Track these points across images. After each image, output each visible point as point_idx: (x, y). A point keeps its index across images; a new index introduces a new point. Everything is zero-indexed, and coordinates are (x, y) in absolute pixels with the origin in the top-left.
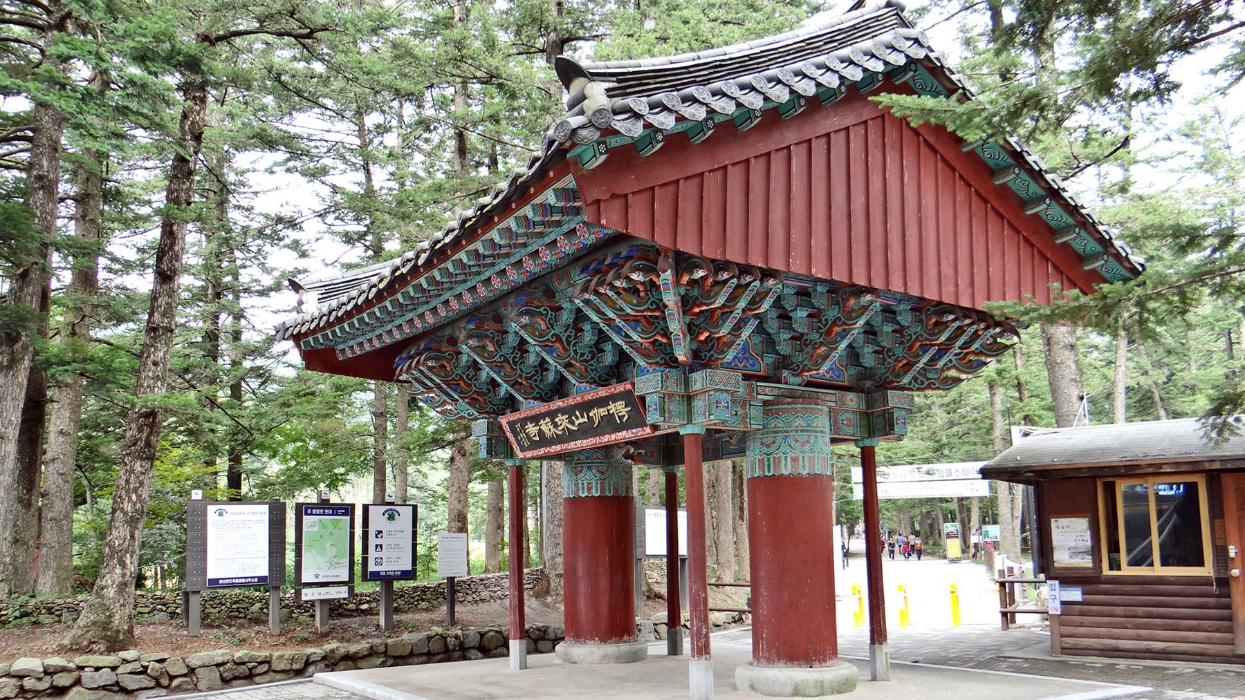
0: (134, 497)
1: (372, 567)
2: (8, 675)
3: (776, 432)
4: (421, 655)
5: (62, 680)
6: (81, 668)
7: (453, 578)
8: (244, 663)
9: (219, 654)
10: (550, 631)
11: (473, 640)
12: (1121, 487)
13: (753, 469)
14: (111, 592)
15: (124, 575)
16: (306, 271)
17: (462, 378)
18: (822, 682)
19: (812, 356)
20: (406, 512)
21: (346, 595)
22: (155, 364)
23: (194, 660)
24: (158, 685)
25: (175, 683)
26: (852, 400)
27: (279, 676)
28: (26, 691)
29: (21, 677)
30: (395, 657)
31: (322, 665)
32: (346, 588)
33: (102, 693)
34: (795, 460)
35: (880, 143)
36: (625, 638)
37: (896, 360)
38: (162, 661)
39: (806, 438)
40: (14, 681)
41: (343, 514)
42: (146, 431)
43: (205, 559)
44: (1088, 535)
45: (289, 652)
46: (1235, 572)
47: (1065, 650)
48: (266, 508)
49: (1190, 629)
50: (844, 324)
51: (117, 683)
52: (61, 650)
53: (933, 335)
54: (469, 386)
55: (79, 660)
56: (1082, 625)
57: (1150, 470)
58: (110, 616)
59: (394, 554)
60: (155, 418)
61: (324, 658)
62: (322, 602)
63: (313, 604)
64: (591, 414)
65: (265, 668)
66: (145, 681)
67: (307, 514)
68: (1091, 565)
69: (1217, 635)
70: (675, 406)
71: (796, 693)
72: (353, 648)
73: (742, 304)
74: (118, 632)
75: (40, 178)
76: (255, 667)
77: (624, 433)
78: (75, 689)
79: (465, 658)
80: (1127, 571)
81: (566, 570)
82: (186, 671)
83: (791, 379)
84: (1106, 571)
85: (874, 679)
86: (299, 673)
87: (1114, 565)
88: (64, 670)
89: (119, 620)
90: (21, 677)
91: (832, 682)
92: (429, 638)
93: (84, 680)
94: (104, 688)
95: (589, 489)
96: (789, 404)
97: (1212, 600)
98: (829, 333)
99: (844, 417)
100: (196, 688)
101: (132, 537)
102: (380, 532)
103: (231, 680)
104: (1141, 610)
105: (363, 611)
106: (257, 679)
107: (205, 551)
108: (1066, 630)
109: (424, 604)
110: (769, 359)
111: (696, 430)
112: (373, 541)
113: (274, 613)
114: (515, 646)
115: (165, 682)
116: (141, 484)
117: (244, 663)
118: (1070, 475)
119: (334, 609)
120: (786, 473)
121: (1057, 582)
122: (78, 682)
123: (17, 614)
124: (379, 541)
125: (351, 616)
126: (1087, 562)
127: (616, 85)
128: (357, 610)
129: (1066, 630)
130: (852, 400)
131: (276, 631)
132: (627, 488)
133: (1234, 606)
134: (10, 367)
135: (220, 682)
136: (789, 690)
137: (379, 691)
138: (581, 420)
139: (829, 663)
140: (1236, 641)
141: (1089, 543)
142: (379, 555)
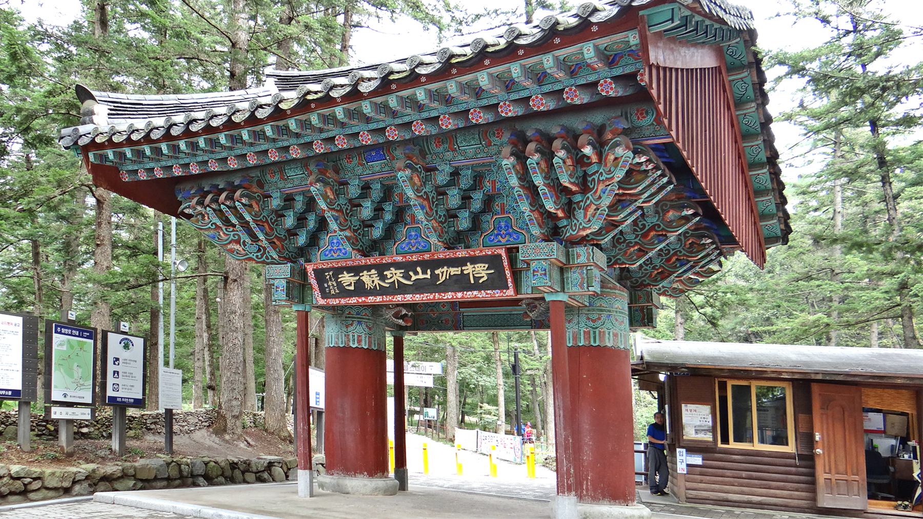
1: (110, 393)
3: (602, 310)
4: (163, 479)
7: (171, 410)
8: (19, 479)
10: (253, 464)
11: (200, 470)
12: (730, 384)
13: (575, 338)
17: (267, 221)
19: (625, 253)
21: (89, 417)
27: (51, 494)
32: (88, 411)
34: (615, 335)
37: (654, 268)
41: (87, 337)
45: (58, 469)
48: (19, 320)
49: (778, 488)
50: (663, 230)
53: (691, 252)
54: (272, 229)
56: (701, 482)
57: (773, 375)
59: (129, 382)
62: (69, 422)
64: (437, 272)
65: (36, 485)
67: (56, 332)
68: (711, 440)
69: (797, 493)
73: (646, 195)
76: (30, 483)
77: (475, 293)
79: (195, 485)
80: (733, 445)
84: (720, 445)
86: (67, 491)
87: (725, 440)
95: (359, 341)
97: (793, 469)
102: (117, 359)
104: (744, 474)
105: (83, 434)
106: (31, 495)
108: (689, 485)
112: (111, 368)
117: (19, 479)
119: (77, 430)
120: (609, 345)
121: (684, 450)
124: (116, 368)
126: (709, 437)
129: (689, 485)
131: (27, 448)
137: (208, 511)
138: (421, 276)
141: (710, 424)
142: (116, 381)
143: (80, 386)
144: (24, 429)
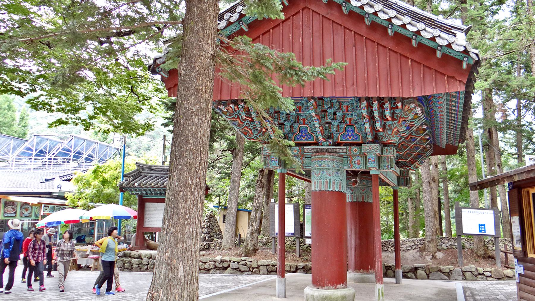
6: (230, 261)
15: (252, 230)
16: (50, 126)
23: (260, 263)
25: (254, 270)
31: (302, 270)
33: (235, 271)
36: (361, 271)
38: (251, 262)
51: (238, 268)
58: (248, 244)
61: (303, 268)
68: (521, 249)
81: (312, 234)
99: (356, 160)
100: (259, 274)
115: (251, 270)
116: (259, 196)
130: (355, 150)
139: (325, 288)
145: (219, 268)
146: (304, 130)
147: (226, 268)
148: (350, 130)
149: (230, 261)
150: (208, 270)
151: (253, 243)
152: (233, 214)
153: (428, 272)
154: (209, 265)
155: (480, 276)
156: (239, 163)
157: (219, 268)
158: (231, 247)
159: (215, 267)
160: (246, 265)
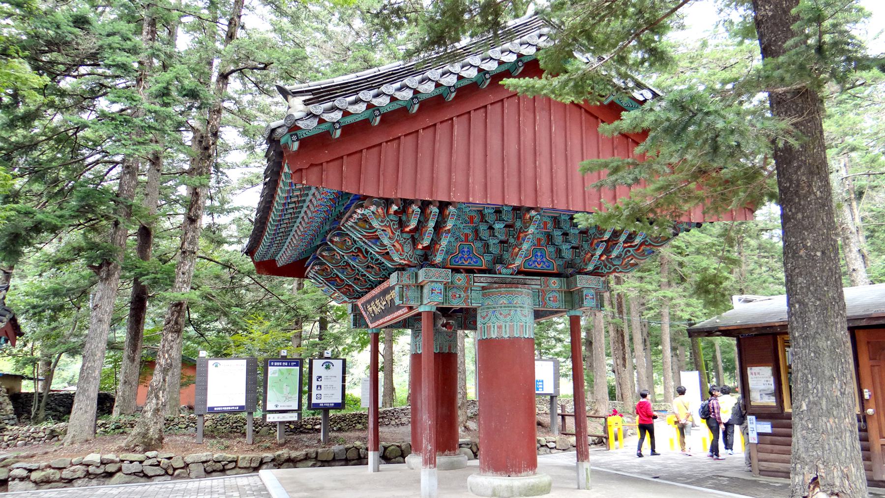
0: (167, 356)
2: (81, 464)
3: (488, 308)
4: (341, 460)
5: (111, 468)
6: (123, 461)
8: (219, 462)
9: (204, 455)
14: (149, 415)
15: (157, 404)
18: (512, 487)
20: (338, 364)
22: (183, 274)
23: (189, 459)
24: (167, 473)
25: (177, 472)
26: (554, 283)
27: (242, 471)
28: (90, 474)
29: (88, 465)
30: (322, 461)
31: (271, 465)
33: (133, 477)
34: (500, 327)
35: (532, 106)
38: (170, 458)
39: (507, 312)
40: (83, 467)
41: (295, 366)
42: (176, 314)
43: (206, 395)
44: (772, 380)
46: (870, 411)
47: (762, 472)
51: (142, 471)
52: (121, 450)
55: (122, 456)
56: (772, 452)
58: (148, 430)
59: (330, 392)
60: (181, 307)
61: (273, 460)
62: (281, 423)
63: (274, 424)
65: (233, 465)
66: (159, 471)
68: (775, 404)
70: (411, 293)
71: (494, 495)
72: (294, 454)
74: (152, 439)
75: (128, 167)
78: (118, 474)
82: (183, 465)
83: (504, 271)
85: (579, 488)
88: (112, 462)
89: (153, 433)
90: (88, 465)
91: (519, 488)
92: (347, 450)
93: (123, 468)
94: (134, 474)
96: (496, 288)
98: (518, 238)
99: (551, 295)
100: (188, 476)
101: (164, 380)
103: (211, 472)
106: (228, 472)
107: (206, 389)
109: (359, 426)
110: (488, 257)
111: (427, 309)
112: (315, 383)
113: (249, 428)
114: (372, 456)
115: (170, 471)
116: (171, 347)
117: (219, 462)
118: (764, 331)
121: (754, 417)
122: (120, 470)
123: (113, 427)
124: (319, 383)
125: (308, 433)
126: (771, 401)
127: (312, 97)
128: (312, 429)
130: (554, 283)
132: (450, 347)
133: (871, 439)
134: (106, 279)
135: (204, 473)
136: (490, 492)
139: (523, 474)
140: (873, 468)
141: (772, 387)
142: (319, 392)
143: (288, 398)
144: (249, 428)
145: (96, 476)
146: (466, 250)
147: (110, 475)
148: (466, 250)
149: (123, 461)
150: (70, 481)
151: (158, 426)
152: (95, 378)
153: (475, 450)
154: (74, 471)
155: (543, 448)
156: (112, 289)
157: (96, 476)
158: (89, 438)
159: (88, 474)
160: (158, 465)
